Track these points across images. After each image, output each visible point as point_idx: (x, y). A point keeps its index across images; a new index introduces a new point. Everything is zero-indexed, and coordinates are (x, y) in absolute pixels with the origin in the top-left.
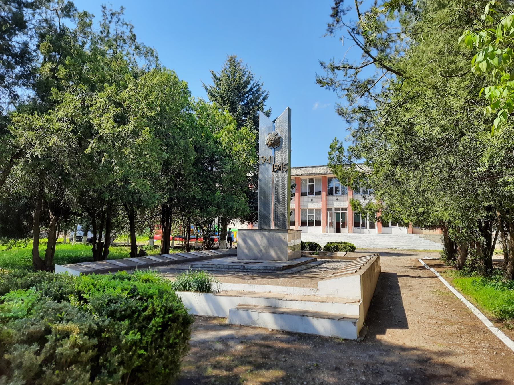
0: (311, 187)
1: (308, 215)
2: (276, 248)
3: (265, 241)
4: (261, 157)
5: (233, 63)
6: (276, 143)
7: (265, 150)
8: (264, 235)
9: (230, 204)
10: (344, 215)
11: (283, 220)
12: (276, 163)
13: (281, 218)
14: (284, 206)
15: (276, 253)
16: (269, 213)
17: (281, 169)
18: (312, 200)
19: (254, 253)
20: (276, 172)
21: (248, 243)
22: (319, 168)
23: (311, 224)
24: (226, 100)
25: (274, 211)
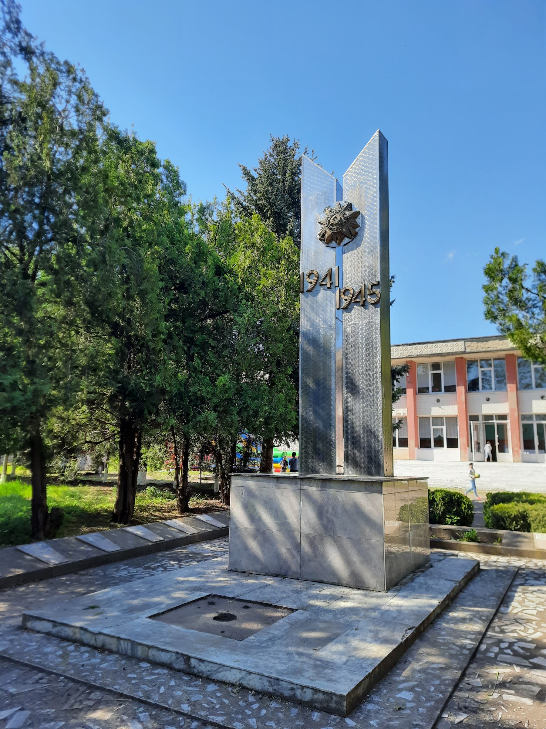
0: (437, 378)
1: (432, 427)
2: (346, 543)
3: (311, 515)
4: (306, 273)
5: (282, 150)
6: (344, 230)
7: (316, 253)
8: (309, 497)
9: (254, 405)
10: (502, 429)
11: (370, 446)
12: (345, 286)
13: (363, 440)
14: (373, 403)
15: (348, 562)
16: (329, 423)
17: (362, 299)
18: (438, 401)
19: (278, 555)
20: (347, 309)
21: (260, 519)
22: (450, 344)
23: (439, 443)
24: (268, 211)
25: (346, 421)
